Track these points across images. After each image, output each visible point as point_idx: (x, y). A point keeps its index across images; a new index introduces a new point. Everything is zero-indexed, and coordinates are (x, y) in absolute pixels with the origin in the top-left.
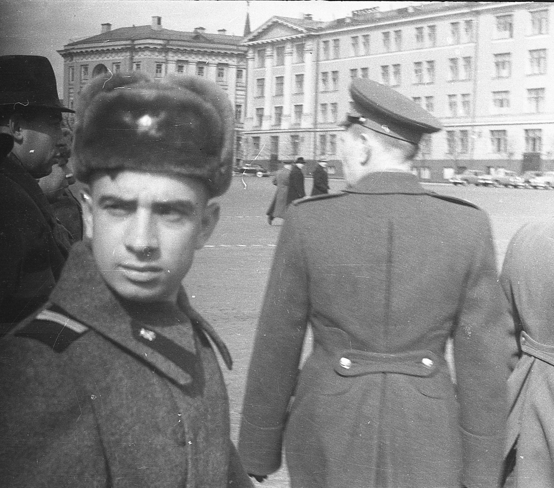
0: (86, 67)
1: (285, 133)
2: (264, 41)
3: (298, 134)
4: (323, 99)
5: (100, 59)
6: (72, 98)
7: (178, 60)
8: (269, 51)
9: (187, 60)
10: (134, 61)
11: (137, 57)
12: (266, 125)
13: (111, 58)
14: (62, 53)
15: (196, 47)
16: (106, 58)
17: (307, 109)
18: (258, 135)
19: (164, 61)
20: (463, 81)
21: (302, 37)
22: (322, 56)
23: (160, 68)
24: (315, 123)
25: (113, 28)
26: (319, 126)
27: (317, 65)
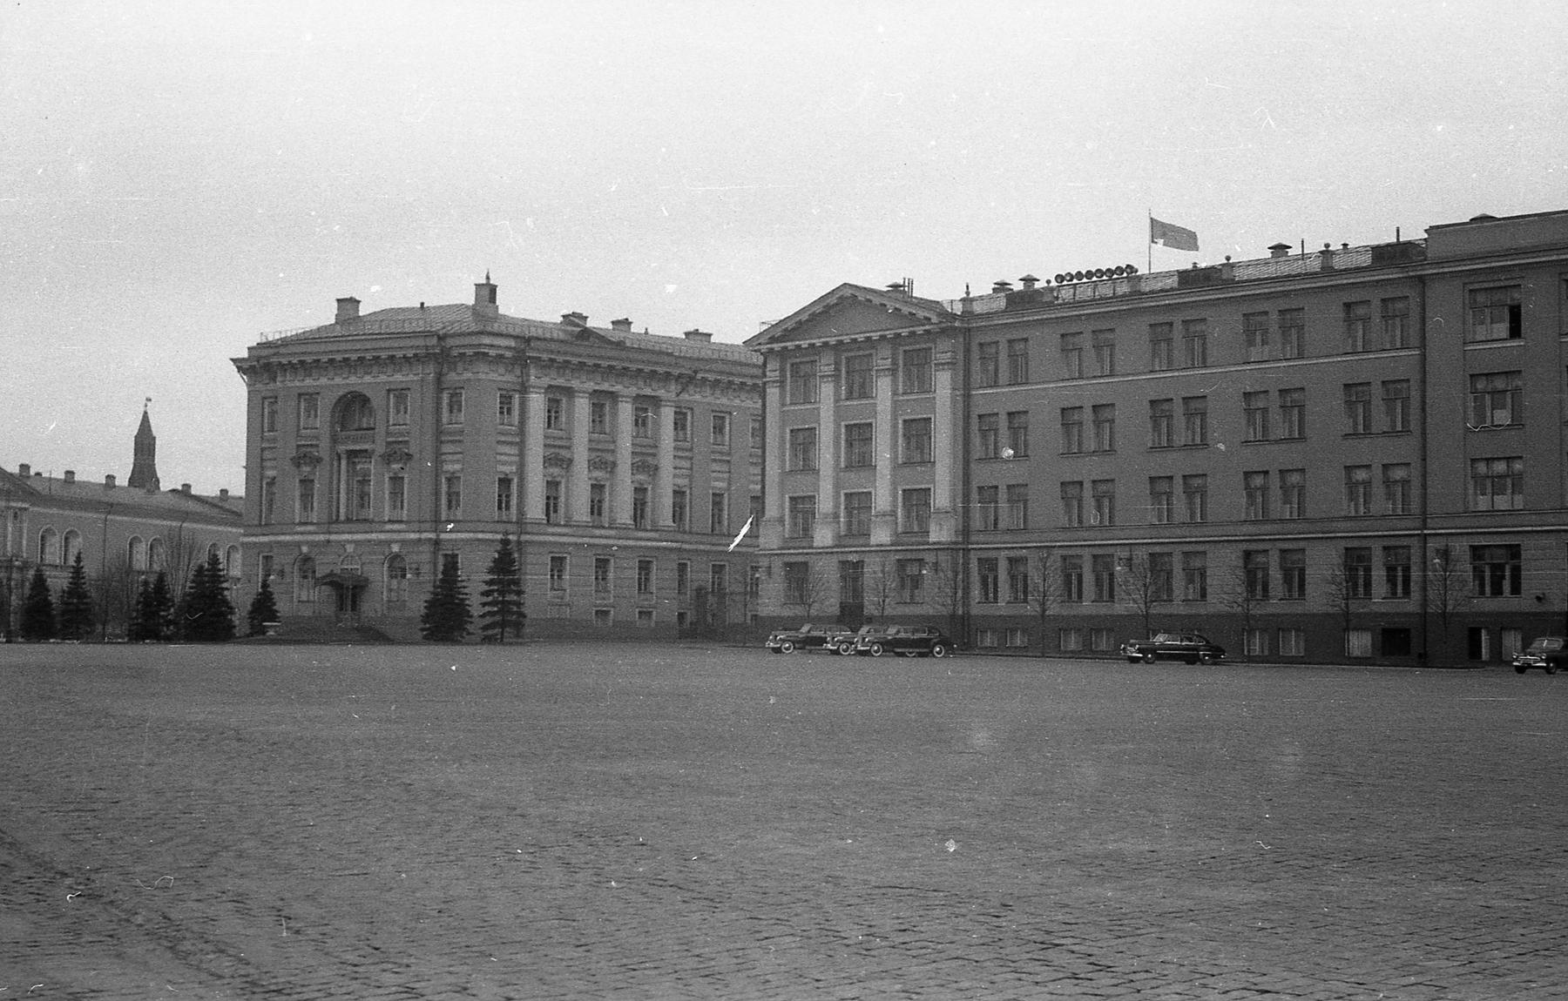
0: (310, 398)
1: (1545, 535)
2: (804, 344)
3: (1111, 550)
4: (983, 475)
5: (353, 379)
6: (270, 473)
7: (595, 391)
8: (825, 365)
9: (613, 389)
10: (445, 386)
11: (452, 377)
12: (823, 536)
13: (383, 378)
14: (245, 366)
15: (739, 375)
16: (368, 379)
17: (942, 497)
18: (1365, 543)
19: (518, 387)
20: (1499, 459)
21: (928, 332)
22: (977, 377)
23: (510, 403)
24: (966, 531)
25: (363, 310)
26: (973, 538)
27: (967, 397)
